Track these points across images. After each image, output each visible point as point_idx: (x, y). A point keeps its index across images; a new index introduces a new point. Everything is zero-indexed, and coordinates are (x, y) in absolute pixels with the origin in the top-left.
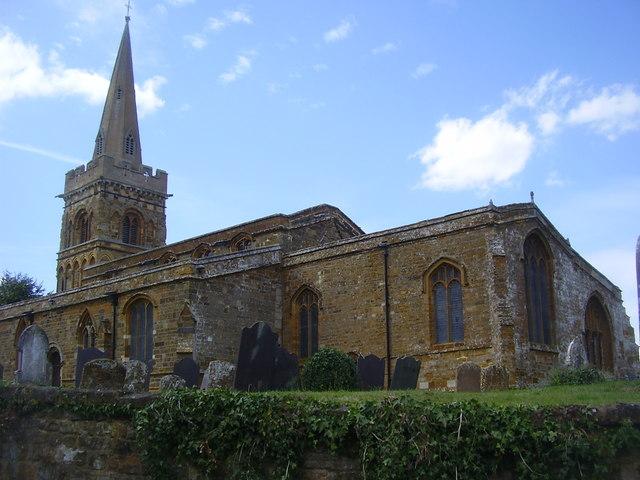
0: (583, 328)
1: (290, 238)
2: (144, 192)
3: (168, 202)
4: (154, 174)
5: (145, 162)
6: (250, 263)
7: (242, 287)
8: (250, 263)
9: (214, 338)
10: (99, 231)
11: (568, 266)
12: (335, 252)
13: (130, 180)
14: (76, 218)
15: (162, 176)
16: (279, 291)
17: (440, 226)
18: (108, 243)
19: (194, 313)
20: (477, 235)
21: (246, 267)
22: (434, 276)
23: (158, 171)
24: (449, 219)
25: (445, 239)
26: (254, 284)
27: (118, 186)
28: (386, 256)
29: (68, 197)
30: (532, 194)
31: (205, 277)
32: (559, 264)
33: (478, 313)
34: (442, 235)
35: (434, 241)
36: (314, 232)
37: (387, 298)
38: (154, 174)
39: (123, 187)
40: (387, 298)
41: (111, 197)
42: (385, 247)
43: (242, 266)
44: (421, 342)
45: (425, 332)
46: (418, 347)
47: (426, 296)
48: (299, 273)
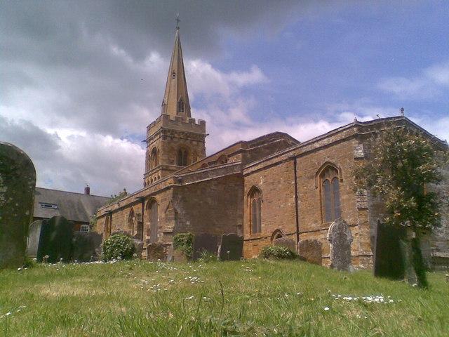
1: (249, 156)
3: (207, 139)
4: (197, 123)
12: (269, 163)
13: (180, 128)
18: (167, 167)
27: (173, 132)
28: (295, 163)
30: (402, 110)
33: (349, 200)
35: (322, 151)
40: (296, 192)
44: (316, 222)
45: (317, 215)
46: (313, 225)
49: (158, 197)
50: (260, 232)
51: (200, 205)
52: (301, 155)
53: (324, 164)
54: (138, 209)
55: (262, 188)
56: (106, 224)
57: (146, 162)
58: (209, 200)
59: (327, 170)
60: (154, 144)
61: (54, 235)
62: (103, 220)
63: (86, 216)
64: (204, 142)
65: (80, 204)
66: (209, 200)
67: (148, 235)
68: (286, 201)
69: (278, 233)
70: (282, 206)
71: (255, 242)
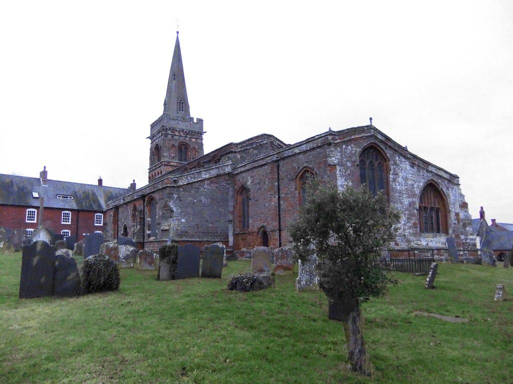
0: (417, 206)
1: (239, 156)
2: (189, 132)
3: (204, 136)
4: (195, 121)
5: (191, 116)
6: (210, 173)
7: (205, 189)
8: (210, 173)
9: (186, 220)
10: (166, 156)
11: (406, 165)
13: (182, 125)
14: (155, 149)
15: (200, 121)
16: (231, 189)
17: (304, 146)
19: (172, 206)
20: (322, 151)
21: (207, 176)
22: (302, 177)
23: (197, 119)
24: (308, 141)
25: (308, 154)
26: (214, 186)
27: (173, 130)
28: (278, 166)
29: (152, 137)
30: (371, 119)
31: (178, 185)
32: (395, 164)
34: (305, 152)
35: (301, 156)
36: (255, 152)
37: (279, 193)
38: (195, 121)
39: (176, 131)
40: (279, 193)
41: (170, 137)
42: (277, 161)
43: (205, 175)
47: (297, 192)
48: (239, 178)
49: (157, 196)
50: (248, 227)
51: (194, 203)
52: (283, 159)
53: (303, 168)
54: (140, 205)
55: (250, 187)
56: (114, 217)
57: (151, 158)
58: (203, 198)
59: (304, 173)
60: (157, 140)
61: (35, 260)
62: (112, 213)
63: (99, 205)
64: (202, 139)
65: (94, 194)
66: (203, 198)
67: (149, 230)
68: (270, 200)
69: (262, 229)
70: (267, 205)
71: (244, 236)
